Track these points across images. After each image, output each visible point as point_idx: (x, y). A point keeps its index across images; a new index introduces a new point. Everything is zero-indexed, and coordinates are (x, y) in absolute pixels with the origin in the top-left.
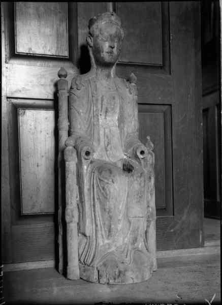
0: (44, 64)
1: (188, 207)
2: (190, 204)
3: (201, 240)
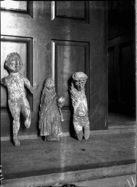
0: (11, 15)
1: (98, 105)
2: (99, 103)
3: (106, 125)
